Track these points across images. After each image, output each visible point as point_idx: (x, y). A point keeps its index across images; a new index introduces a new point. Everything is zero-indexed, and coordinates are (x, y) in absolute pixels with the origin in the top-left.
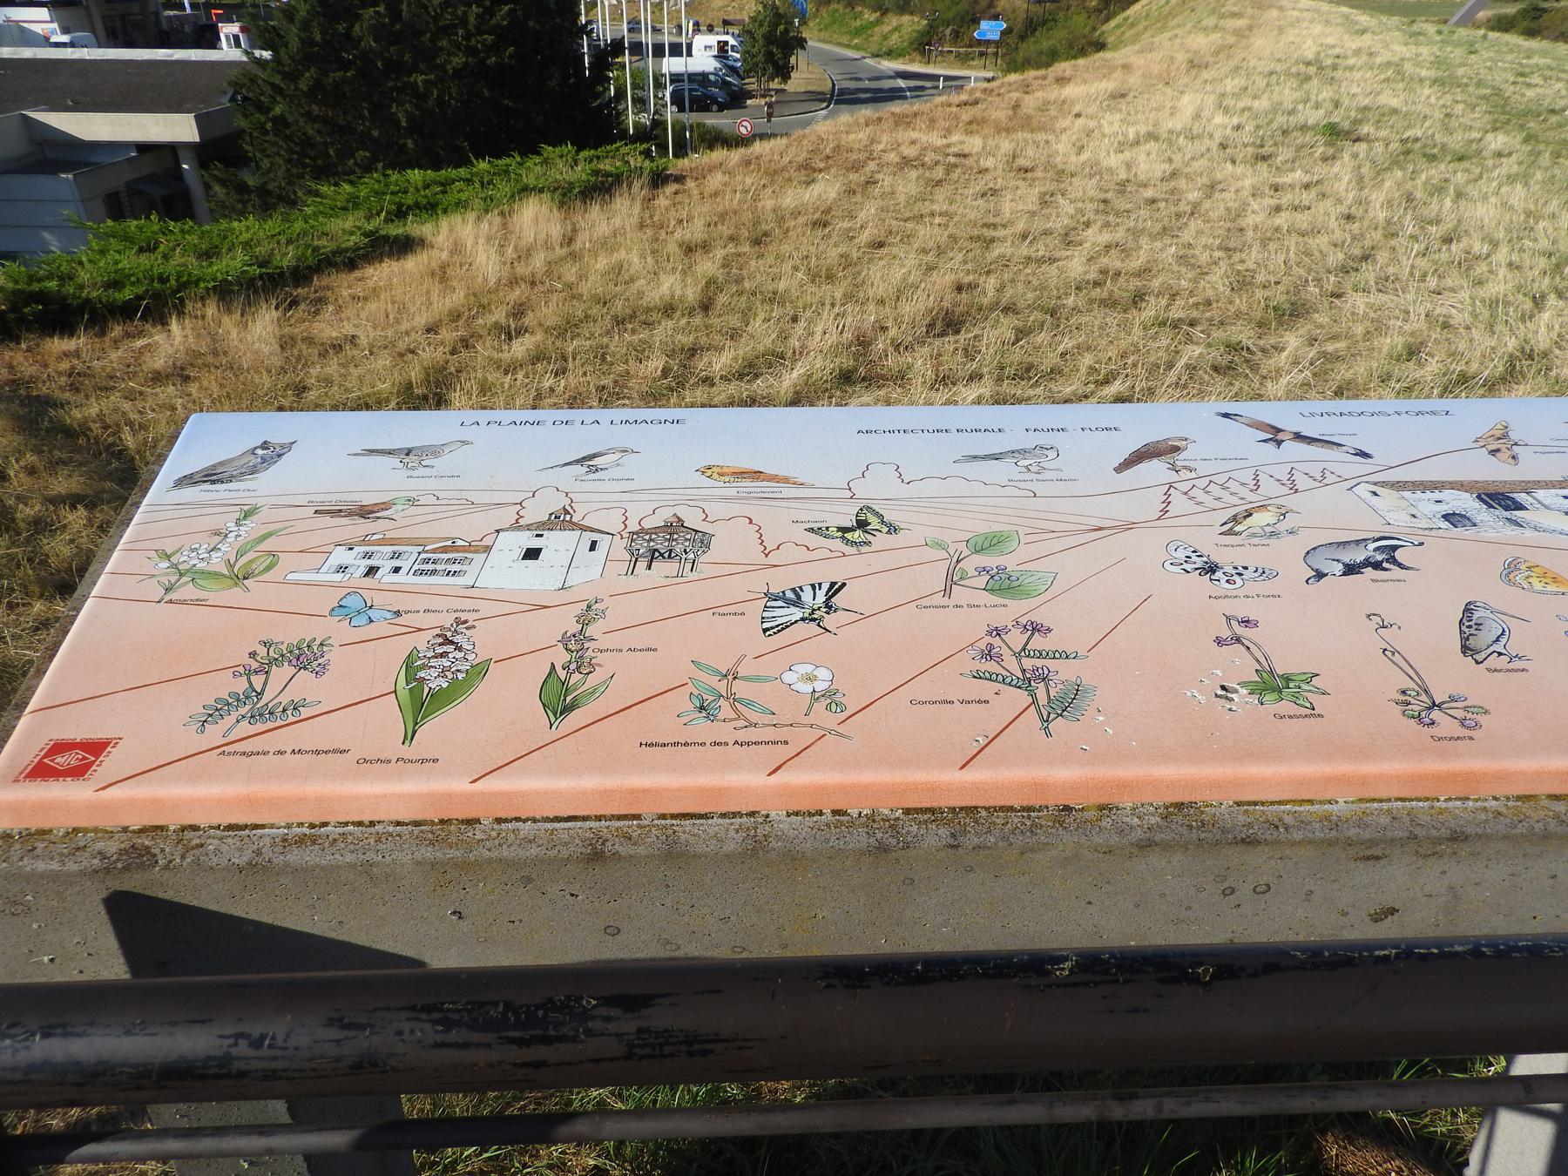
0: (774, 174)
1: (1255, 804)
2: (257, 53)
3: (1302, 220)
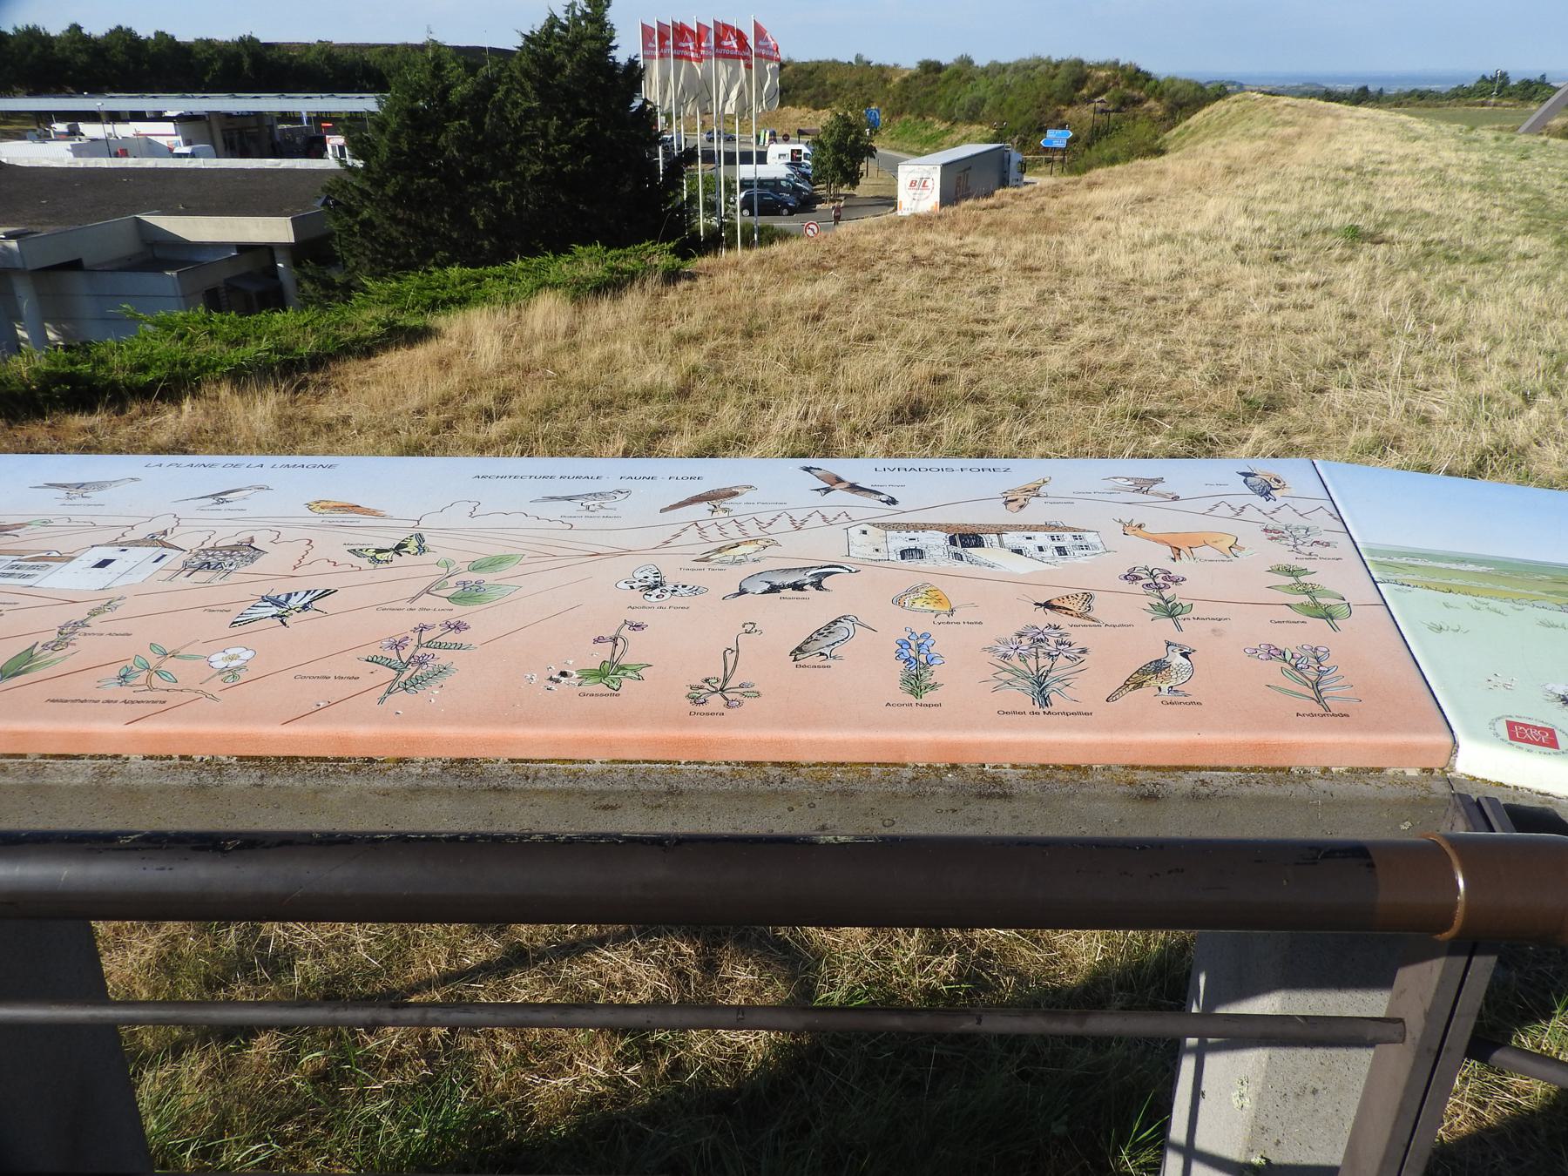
0: (785, 273)
1: (527, 761)
2: (350, 162)
3: (1300, 319)
